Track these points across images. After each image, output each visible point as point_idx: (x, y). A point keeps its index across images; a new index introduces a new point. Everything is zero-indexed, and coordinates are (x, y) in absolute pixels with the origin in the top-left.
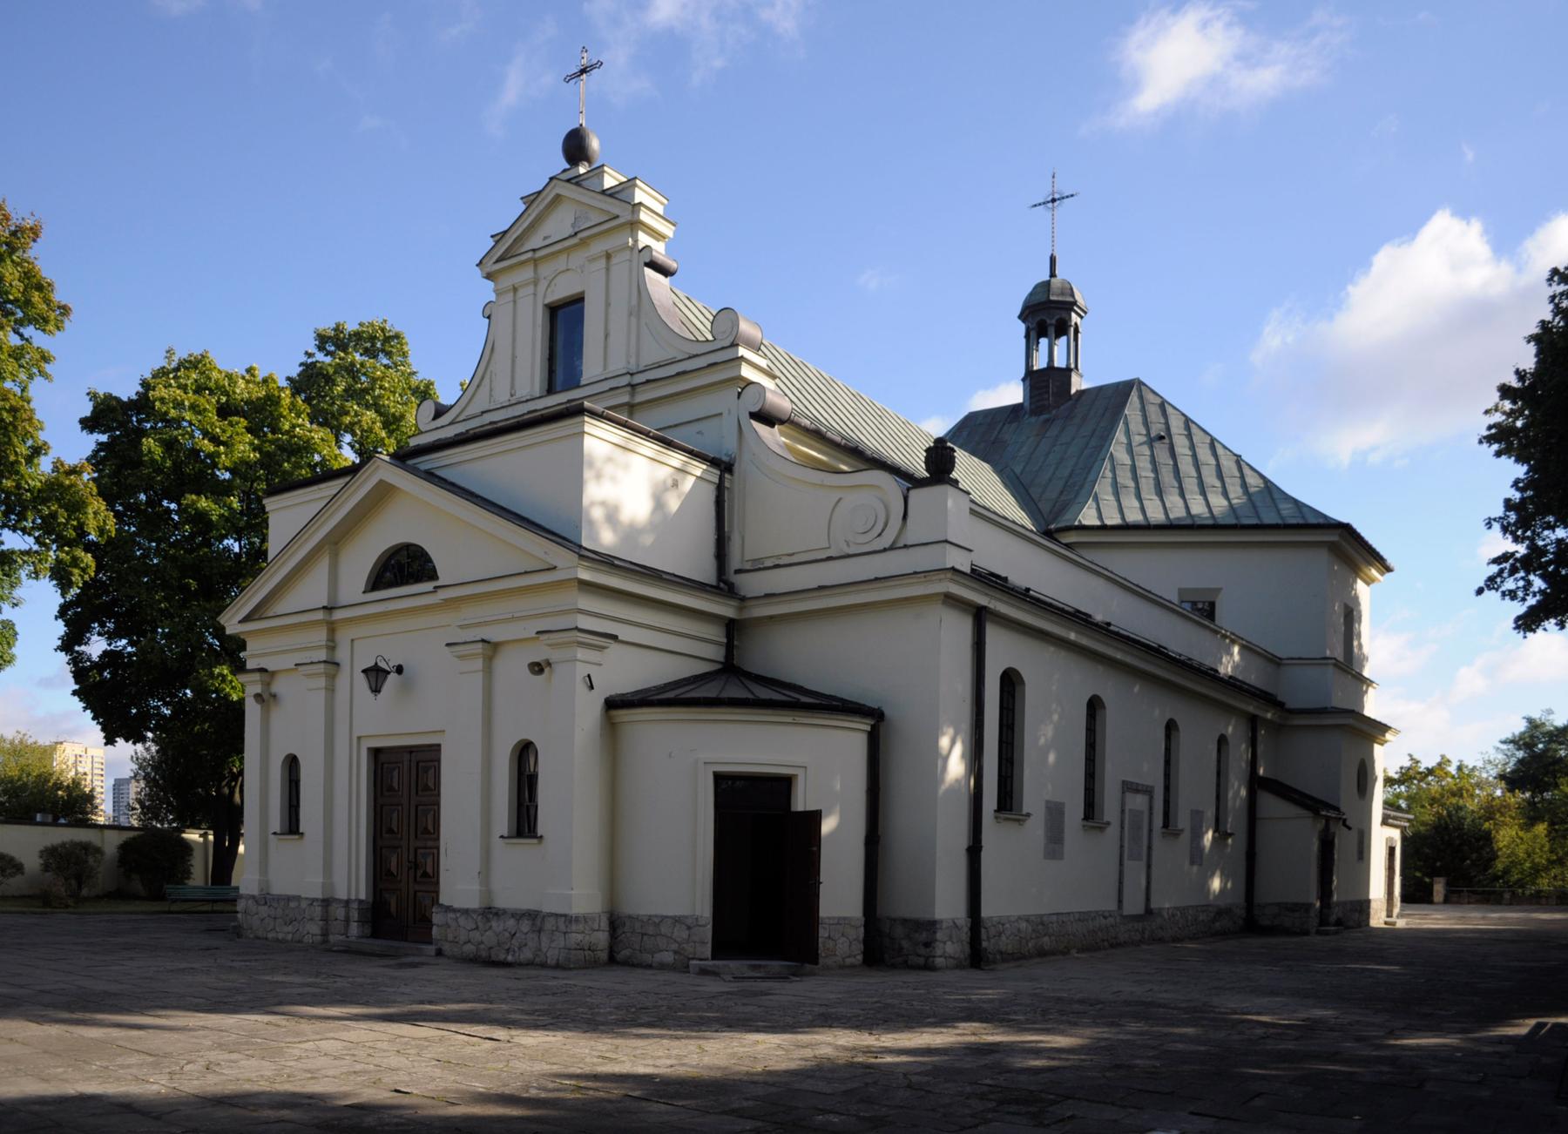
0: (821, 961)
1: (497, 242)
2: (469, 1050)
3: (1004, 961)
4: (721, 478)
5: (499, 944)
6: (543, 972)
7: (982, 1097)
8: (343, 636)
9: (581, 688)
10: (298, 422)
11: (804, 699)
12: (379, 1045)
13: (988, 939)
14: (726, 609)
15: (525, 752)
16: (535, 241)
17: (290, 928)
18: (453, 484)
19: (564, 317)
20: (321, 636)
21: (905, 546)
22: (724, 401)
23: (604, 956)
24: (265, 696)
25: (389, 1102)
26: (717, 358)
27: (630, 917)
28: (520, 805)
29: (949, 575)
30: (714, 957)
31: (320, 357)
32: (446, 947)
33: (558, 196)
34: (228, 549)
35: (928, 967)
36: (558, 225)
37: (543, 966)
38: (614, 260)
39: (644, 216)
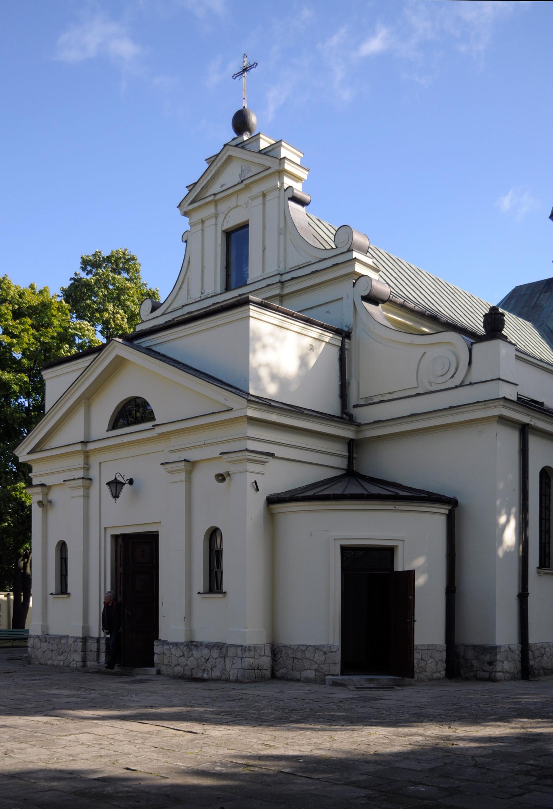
0: (416, 675)
1: (190, 191)
2: (176, 740)
3: (545, 674)
4: (343, 343)
5: (198, 666)
6: (228, 685)
7: (527, 773)
8: (94, 461)
9: (250, 490)
10: (62, 319)
11: (402, 493)
12: (117, 737)
13: (534, 659)
14: (347, 433)
15: (214, 534)
16: (215, 188)
17: (62, 658)
18: (164, 356)
19: (236, 239)
20: (80, 461)
21: (471, 384)
22: (343, 289)
23: (268, 673)
24: (45, 503)
25: (122, 776)
26: (339, 260)
27: (285, 646)
28: (211, 571)
29: (502, 403)
30: (342, 674)
31: (83, 275)
32: (163, 669)
33: (230, 158)
34: (21, 405)
35: (492, 679)
36: (231, 176)
37: (227, 680)
38: (268, 198)
39: (288, 166)
